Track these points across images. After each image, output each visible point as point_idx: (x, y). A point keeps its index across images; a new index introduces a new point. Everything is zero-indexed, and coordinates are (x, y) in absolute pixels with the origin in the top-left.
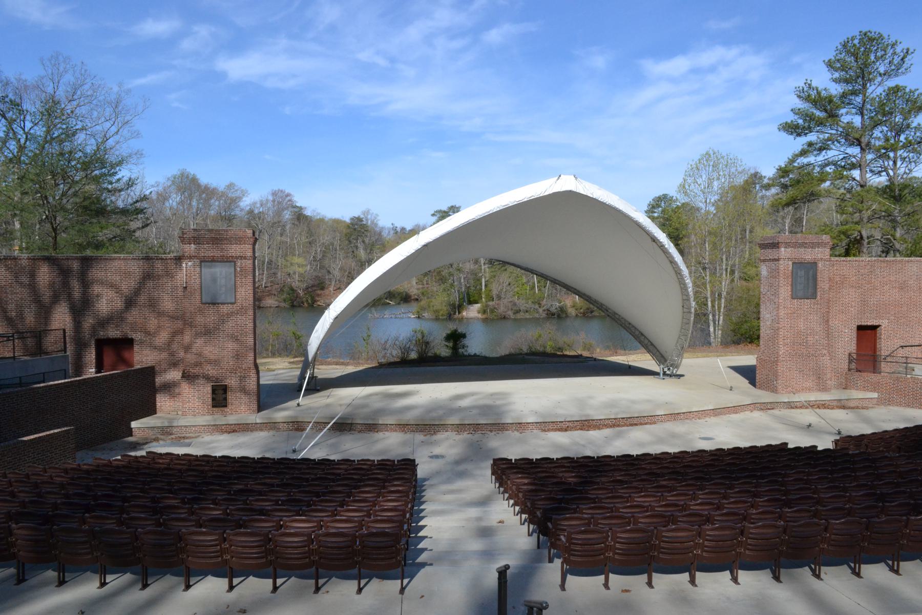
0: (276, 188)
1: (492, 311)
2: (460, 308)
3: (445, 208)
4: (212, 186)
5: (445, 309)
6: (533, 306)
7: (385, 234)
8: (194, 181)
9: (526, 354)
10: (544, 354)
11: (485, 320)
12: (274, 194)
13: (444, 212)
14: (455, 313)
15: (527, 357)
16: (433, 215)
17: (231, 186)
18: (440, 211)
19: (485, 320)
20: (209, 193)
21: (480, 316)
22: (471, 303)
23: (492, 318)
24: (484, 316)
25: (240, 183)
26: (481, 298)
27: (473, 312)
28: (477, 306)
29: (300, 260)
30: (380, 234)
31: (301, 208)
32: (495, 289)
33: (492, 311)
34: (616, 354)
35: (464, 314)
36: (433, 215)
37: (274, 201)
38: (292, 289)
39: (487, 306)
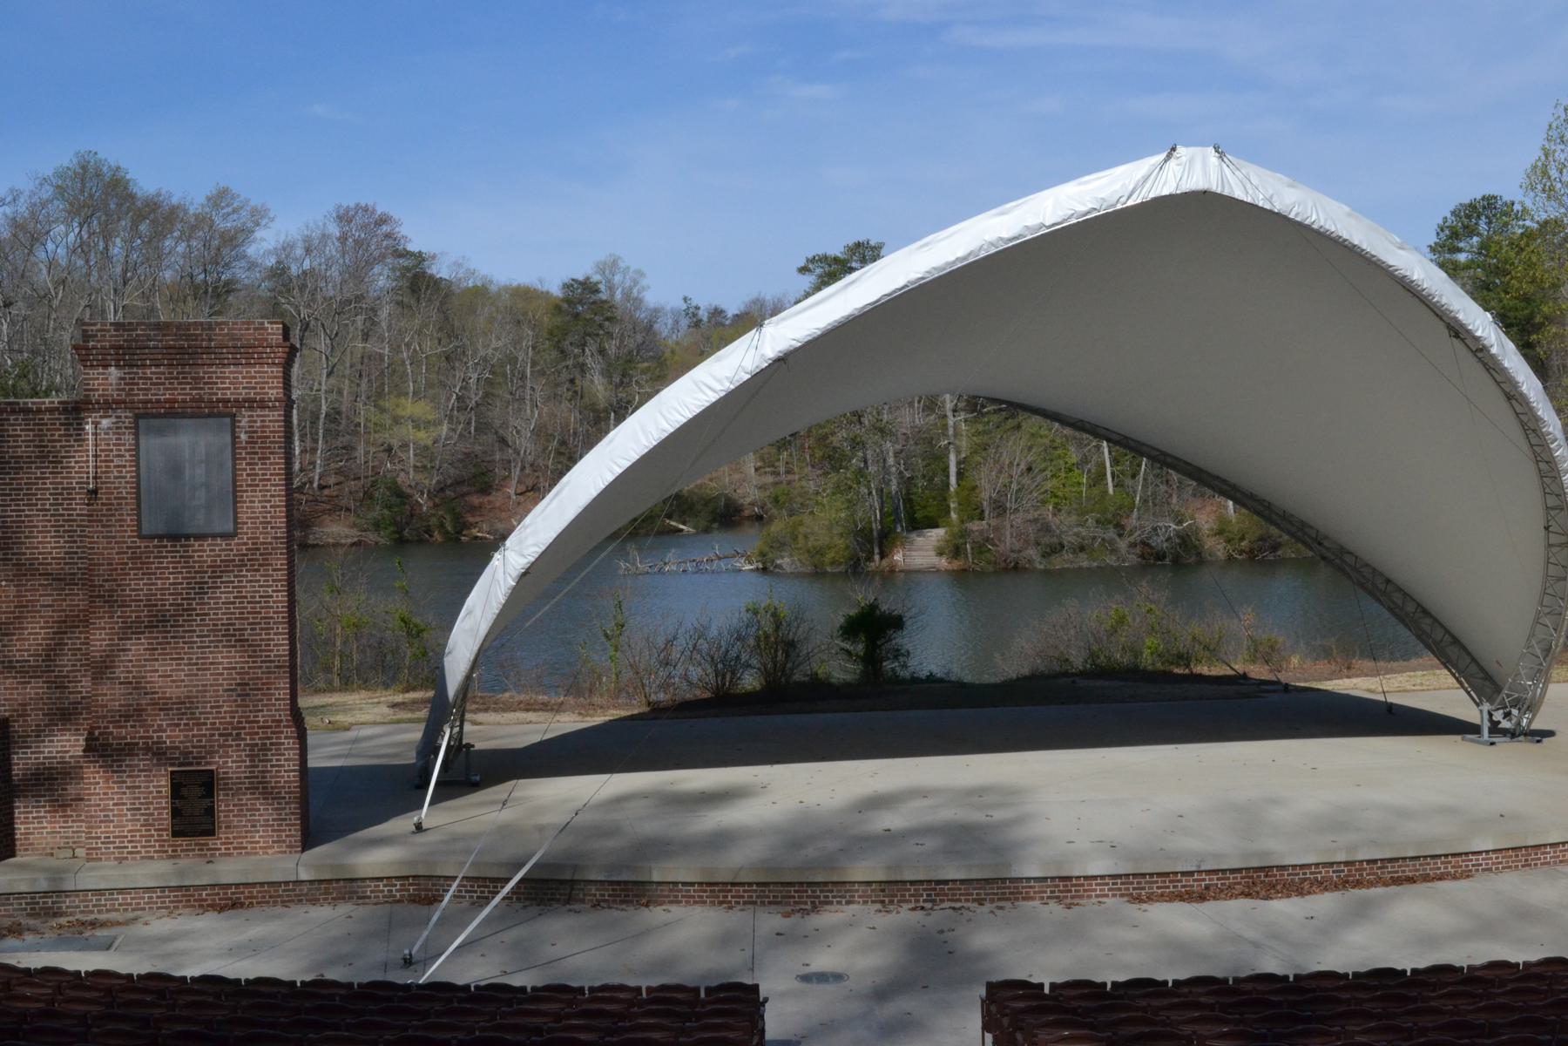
1: (980, 549)
2: (885, 540)
6: (1100, 533)
8: (117, 186)
9: (1083, 674)
10: (1134, 674)
12: (344, 218)
13: (836, 260)
14: (870, 559)
15: (1081, 683)
16: (803, 270)
17: (220, 198)
18: (824, 259)
20: (158, 217)
21: (943, 563)
22: (918, 524)
23: (981, 571)
24: (956, 565)
27: (922, 551)
28: (936, 535)
29: (411, 408)
30: (649, 328)
31: (420, 257)
33: (980, 549)
34: (1348, 670)
35: (898, 557)
36: (803, 270)
39: (964, 534)
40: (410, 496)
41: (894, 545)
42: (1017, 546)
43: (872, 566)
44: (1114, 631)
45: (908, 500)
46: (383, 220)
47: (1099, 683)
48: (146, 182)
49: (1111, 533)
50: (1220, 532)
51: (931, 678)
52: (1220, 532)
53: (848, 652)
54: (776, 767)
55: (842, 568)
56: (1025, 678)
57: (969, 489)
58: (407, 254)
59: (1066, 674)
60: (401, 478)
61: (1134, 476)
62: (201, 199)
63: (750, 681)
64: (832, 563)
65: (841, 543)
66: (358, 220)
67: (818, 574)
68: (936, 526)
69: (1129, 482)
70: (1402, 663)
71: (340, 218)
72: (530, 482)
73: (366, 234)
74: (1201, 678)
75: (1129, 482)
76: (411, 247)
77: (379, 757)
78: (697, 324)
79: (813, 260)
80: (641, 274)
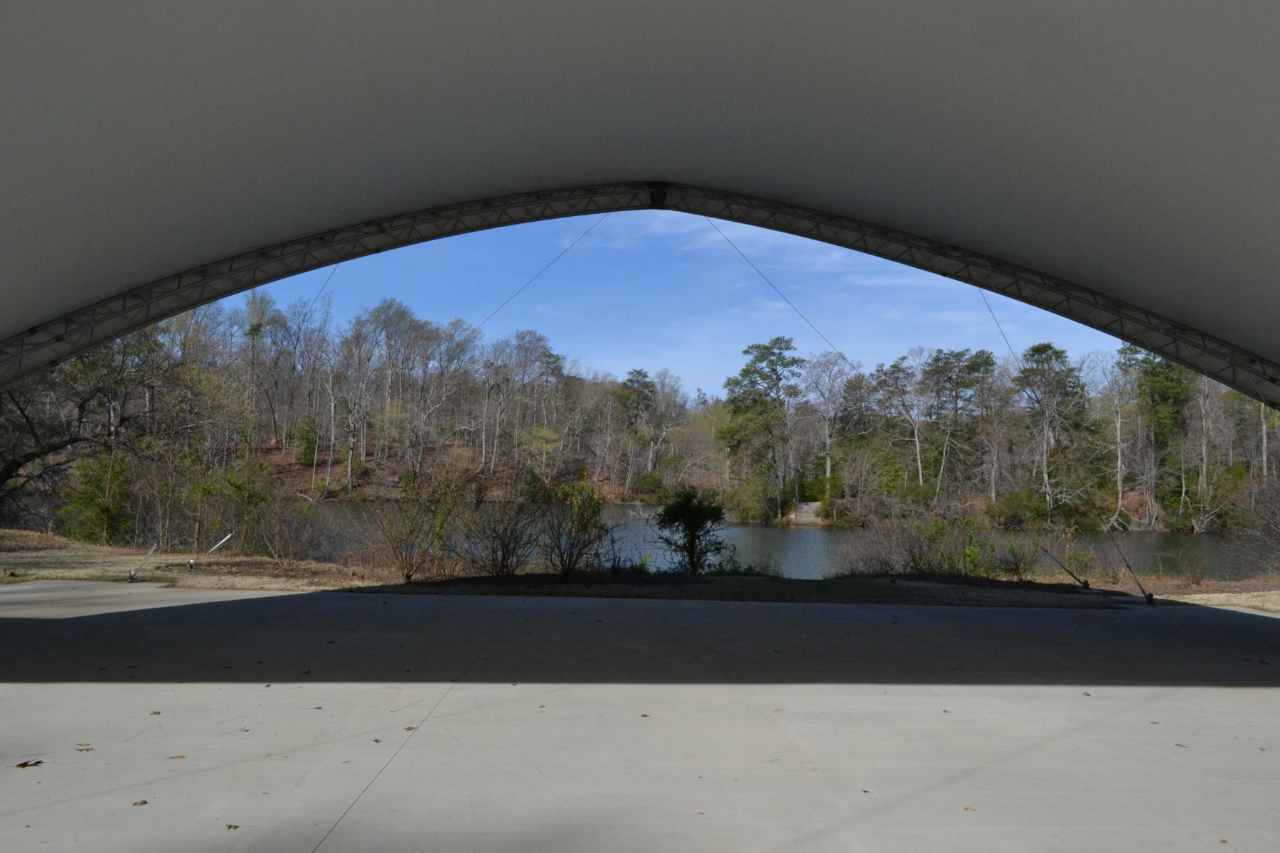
0: (523, 329)
1: (841, 513)
2: (785, 506)
3: (765, 341)
4: (434, 326)
5: (757, 505)
6: (913, 507)
7: (688, 406)
8: (402, 314)
9: (900, 576)
10: (954, 578)
11: (828, 528)
12: (521, 336)
13: (765, 347)
14: (776, 516)
15: (905, 583)
16: (746, 352)
17: (457, 324)
18: (758, 347)
19: (828, 528)
20: (423, 335)
21: (819, 521)
22: (805, 499)
23: (839, 523)
24: (827, 522)
25: (472, 321)
26: (824, 492)
27: (807, 514)
28: (815, 505)
29: (546, 433)
30: (683, 407)
31: (557, 358)
32: (847, 478)
33: (841, 513)
34: (1196, 582)
35: (792, 516)
36: (746, 352)
37: (519, 347)
38: (534, 477)
39: (832, 504)
40: (540, 480)
41: (790, 509)
42: (864, 512)
43: (777, 521)
44: (932, 540)
45: (802, 486)
46: (540, 339)
47: (920, 584)
48: (421, 315)
49: (922, 509)
50: (987, 513)
51: (749, 572)
52: (987, 513)
53: (668, 542)
54: (277, 687)
55: (758, 521)
56: (845, 577)
57: (835, 479)
58: (551, 356)
59: (886, 575)
60: (537, 471)
61: (936, 476)
62: (446, 324)
63: (535, 562)
64: (753, 518)
65: (757, 505)
66: (527, 339)
67: (744, 523)
68: (815, 500)
69: (933, 480)
70: (1233, 583)
71: (518, 337)
72: (606, 475)
73: (532, 347)
74: (1031, 585)
75: (933, 480)
76: (554, 353)
77: (1254, 607)
78: (705, 402)
79: (752, 347)
80: (679, 379)
